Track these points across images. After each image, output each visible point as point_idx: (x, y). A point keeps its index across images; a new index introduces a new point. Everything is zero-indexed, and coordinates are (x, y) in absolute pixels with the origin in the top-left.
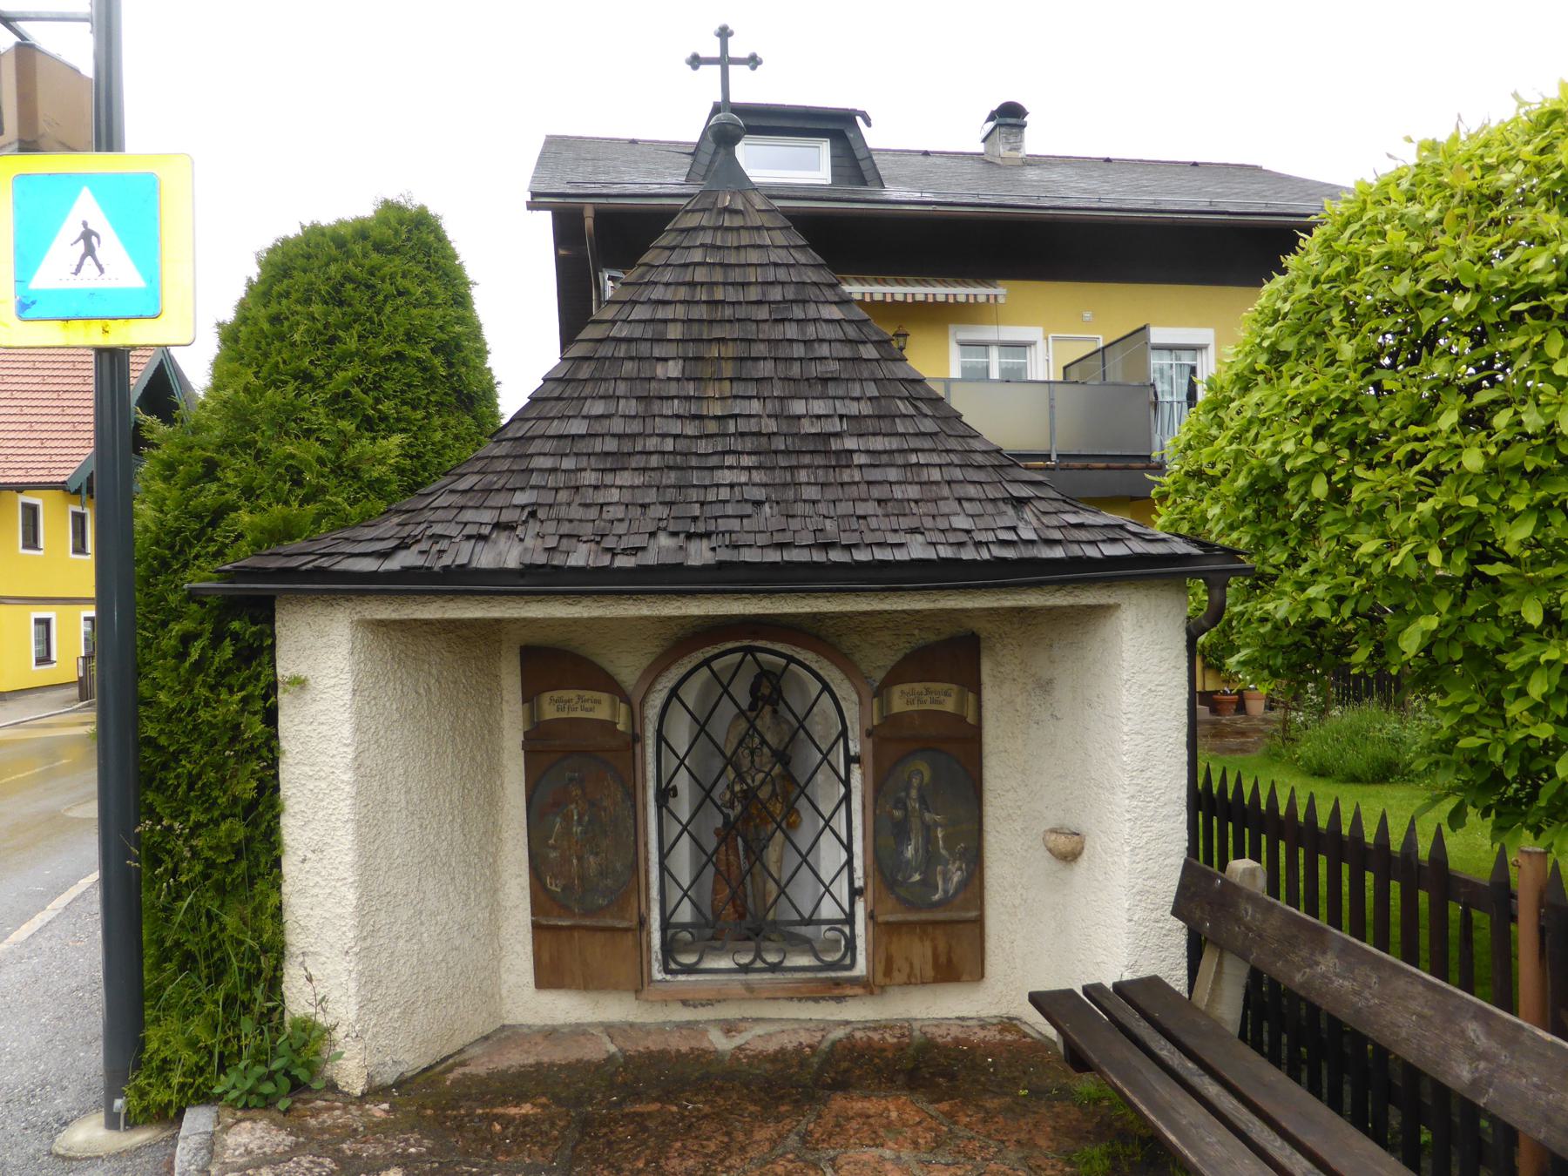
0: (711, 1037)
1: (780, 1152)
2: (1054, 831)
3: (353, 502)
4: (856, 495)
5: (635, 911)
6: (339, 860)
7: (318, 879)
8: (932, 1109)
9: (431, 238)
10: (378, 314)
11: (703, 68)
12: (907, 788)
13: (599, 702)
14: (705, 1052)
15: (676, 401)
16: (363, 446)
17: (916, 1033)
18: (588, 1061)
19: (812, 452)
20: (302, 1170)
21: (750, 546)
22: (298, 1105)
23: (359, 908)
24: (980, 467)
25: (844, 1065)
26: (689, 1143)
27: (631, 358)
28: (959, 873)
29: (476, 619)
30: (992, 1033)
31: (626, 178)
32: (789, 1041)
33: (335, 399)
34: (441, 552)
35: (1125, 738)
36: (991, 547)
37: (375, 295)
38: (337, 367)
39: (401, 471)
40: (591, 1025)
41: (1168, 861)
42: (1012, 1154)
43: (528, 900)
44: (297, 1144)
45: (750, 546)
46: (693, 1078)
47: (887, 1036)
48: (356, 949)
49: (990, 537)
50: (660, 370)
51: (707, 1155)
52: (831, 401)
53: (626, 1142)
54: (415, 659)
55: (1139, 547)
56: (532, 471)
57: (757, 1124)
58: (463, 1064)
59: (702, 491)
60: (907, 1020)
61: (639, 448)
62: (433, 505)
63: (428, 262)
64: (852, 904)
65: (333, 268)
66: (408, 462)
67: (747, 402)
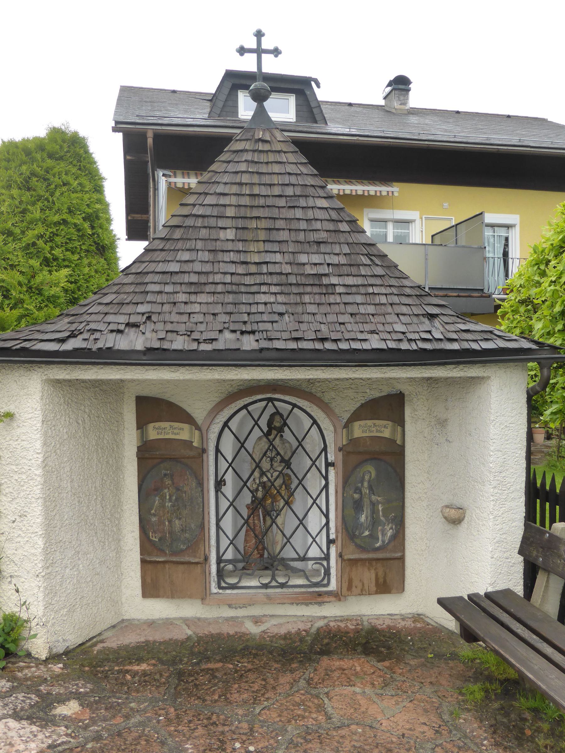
0: (246, 626)
1: (296, 689)
2: (447, 507)
3: (40, 309)
4: (338, 311)
5: (203, 552)
6: (33, 521)
7: (20, 532)
8: (380, 665)
9: (82, 151)
10: (52, 196)
11: (246, 55)
12: (362, 482)
13: (183, 429)
14: (244, 634)
15: (232, 253)
16: (43, 276)
17: (365, 623)
18: (176, 640)
19: (312, 285)
20: (19, 701)
21: (278, 339)
22: (10, 665)
23: (45, 549)
24: (409, 296)
25: (326, 641)
26: (243, 685)
27: (205, 227)
28: (391, 531)
29: (110, 380)
30: (409, 623)
31: (172, 114)
32: (293, 628)
33: (27, 247)
34: (96, 339)
35: (492, 453)
36: (417, 342)
37: (49, 185)
38: (28, 228)
39: (66, 291)
40: (175, 619)
41: (514, 524)
42: (428, 690)
43: (138, 545)
44: (13, 687)
45: (278, 339)
46: (239, 649)
47: (348, 624)
48: (43, 574)
49: (416, 336)
50: (222, 235)
51: (253, 692)
52: (322, 255)
53: (205, 684)
54: (76, 403)
55: (502, 344)
56: (147, 292)
57: (280, 674)
58: (102, 641)
59: (248, 306)
60: (360, 616)
61: (210, 280)
62: (89, 311)
63: (80, 165)
64: (328, 549)
65: (24, 168)
66: (69, 285)
67: (273, 254)
